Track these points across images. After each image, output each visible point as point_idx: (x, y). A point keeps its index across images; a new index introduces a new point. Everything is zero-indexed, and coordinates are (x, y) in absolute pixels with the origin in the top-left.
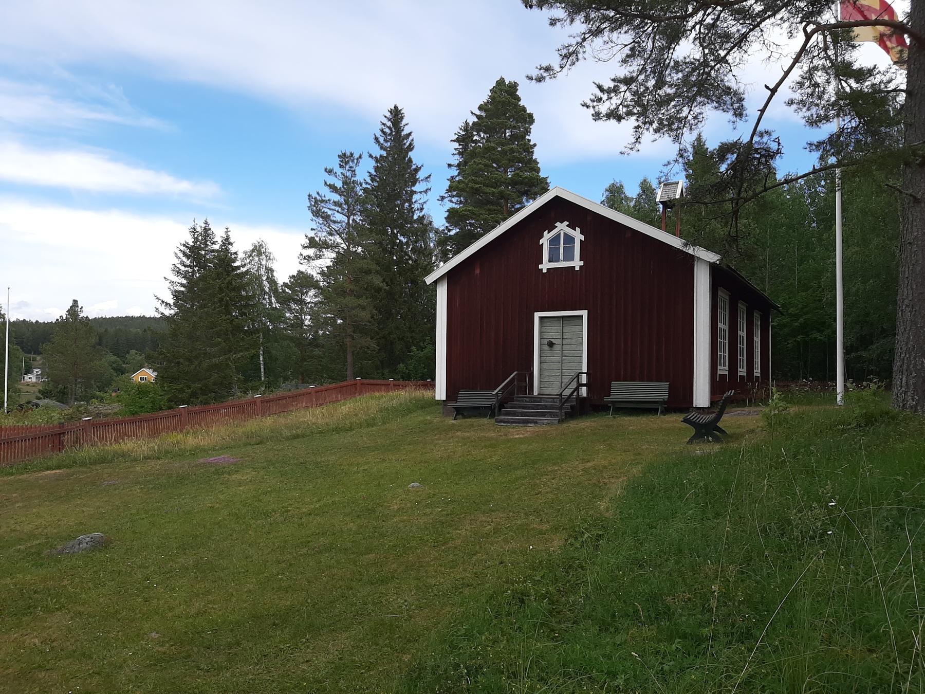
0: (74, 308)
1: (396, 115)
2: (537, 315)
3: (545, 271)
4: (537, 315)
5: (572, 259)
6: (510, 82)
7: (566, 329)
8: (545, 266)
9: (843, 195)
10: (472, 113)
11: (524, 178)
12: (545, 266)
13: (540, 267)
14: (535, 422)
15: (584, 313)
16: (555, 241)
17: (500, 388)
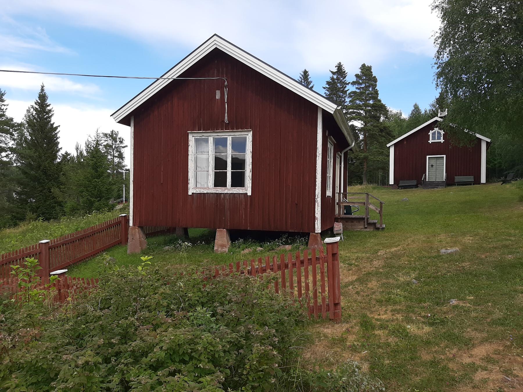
0: (124, 157)
1: (305, 72)
2: (428, 157)
3: (444, 141)
4: (428, 157)
5: (440, 139)
6: (377, 89)
8: (430, 141)
10: (330, 71)
11: (378, 105)
12: (430, 141)
13: (442, 142)
14: (437, 188)
15: (445, 156)
16: (434, 134)
17: (131, 218)
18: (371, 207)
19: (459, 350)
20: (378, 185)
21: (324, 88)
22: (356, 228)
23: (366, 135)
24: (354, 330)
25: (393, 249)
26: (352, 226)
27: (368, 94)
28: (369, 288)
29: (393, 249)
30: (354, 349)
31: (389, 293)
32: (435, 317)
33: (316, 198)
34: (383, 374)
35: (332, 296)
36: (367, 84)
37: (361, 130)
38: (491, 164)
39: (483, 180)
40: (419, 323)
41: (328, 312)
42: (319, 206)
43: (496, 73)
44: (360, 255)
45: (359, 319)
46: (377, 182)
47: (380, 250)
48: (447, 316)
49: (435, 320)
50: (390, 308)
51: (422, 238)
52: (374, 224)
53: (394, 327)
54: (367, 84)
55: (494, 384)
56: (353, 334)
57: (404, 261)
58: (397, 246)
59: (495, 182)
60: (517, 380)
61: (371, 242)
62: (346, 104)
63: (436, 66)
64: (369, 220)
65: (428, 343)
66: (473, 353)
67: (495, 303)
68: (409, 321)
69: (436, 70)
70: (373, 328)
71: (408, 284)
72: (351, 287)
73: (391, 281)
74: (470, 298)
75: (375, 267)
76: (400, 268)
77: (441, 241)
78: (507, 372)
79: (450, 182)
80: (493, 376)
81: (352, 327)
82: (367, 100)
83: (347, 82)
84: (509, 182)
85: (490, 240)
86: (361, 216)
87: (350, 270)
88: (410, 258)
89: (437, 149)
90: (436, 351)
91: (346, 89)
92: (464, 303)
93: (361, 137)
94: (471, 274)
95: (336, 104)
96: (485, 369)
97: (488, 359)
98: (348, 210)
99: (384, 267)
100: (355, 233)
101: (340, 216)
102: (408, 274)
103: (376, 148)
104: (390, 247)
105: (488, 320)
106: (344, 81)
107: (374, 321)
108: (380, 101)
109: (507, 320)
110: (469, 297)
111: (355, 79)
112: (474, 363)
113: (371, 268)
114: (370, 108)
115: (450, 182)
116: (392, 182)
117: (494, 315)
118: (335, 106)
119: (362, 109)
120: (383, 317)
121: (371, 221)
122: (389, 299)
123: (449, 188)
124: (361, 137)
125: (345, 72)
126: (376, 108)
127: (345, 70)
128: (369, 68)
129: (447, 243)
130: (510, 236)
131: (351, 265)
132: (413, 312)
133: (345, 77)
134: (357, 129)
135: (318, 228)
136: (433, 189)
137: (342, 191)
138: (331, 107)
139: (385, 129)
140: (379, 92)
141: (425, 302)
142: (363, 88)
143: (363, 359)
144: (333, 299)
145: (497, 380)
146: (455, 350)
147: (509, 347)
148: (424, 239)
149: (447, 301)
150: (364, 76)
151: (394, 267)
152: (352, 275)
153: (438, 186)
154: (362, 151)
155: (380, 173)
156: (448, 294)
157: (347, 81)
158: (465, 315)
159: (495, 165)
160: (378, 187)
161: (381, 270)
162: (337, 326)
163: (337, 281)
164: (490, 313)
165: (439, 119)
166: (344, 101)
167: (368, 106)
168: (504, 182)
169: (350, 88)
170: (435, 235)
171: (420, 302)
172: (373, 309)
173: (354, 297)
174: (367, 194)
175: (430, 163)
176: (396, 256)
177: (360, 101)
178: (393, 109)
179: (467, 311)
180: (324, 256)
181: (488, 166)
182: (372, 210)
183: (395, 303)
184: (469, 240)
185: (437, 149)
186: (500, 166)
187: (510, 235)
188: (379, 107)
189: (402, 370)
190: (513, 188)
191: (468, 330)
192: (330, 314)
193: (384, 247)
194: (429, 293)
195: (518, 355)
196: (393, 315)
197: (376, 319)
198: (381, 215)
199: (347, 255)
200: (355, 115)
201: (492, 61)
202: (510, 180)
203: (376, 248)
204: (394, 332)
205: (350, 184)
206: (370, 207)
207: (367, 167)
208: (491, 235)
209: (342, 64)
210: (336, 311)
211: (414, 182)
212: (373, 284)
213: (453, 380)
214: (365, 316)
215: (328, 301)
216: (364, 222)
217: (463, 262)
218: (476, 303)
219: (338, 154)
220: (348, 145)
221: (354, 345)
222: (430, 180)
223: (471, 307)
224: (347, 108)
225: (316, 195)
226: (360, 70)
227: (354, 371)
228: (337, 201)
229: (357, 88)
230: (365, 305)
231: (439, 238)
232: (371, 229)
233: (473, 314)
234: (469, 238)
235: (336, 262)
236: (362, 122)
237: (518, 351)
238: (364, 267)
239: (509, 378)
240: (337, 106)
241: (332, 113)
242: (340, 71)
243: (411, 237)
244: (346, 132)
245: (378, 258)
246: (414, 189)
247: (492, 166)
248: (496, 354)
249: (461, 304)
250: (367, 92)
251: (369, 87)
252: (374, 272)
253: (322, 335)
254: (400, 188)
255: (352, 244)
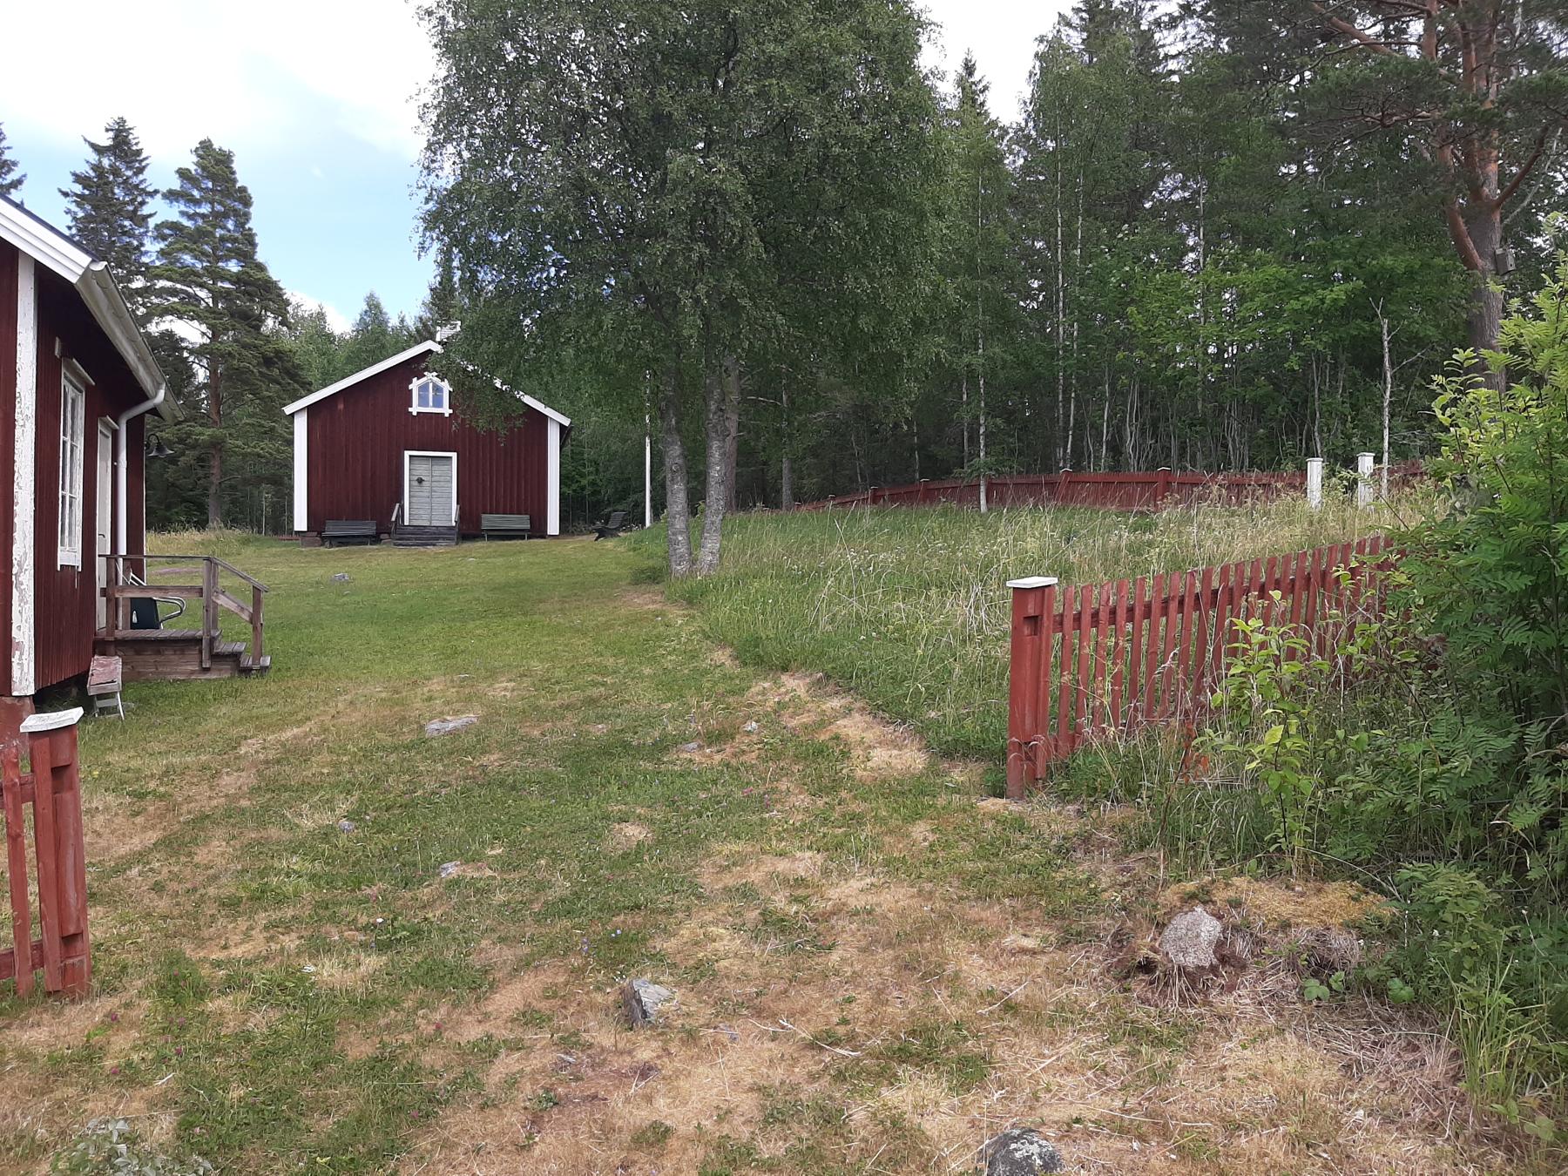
2: (407, 454)
4: (407, 454)
6: (250, 229)
7: (435, 468)
8: (415, 409)
9: (533, 394)
12: (415, 409)
15: (454, 455)
16: (423, 388)
18: (222, 601)
19: (455, 1006)
20: (260, 532)
21: (66, 194)
22: (170, 673)
23: (215, 371)
24: (133, 1014)
25: (288, 734)
26: (156, 665)
27: (223, 239)
28: (197, 866)
29: (288, 734)
30: (128, 1077)
31: (263, 873)
32: (395, 924)
33: (14, 571)
34: (220, 1137)
35: (55, 912)
36: (218, 208)
37: (199, 352)
38: (574, 486)
39: (553, 526)
40: (348, 950)
41: (40, 971)
42: (26, 603)
43: (576, 241)
44: (175, 760)
45: (155, 972)
46: (255, 523)
47: (246, 738)
48: (430, 915)
49: (395, 933)
50: (262, 918)
51: (379, 691)
52: (235, 656)
53: (268, 977)
54: (218, 208)
55: (535, 1081)
56: (131, 1029)
57: (319, 765)
58: (300, 723)
59: (581, 533)
60: (589, 1056)
61: (220, 716)
62: (145, 259)
63: (424, 193)
64: (216, 644)
65: (369, 1005)
66: (490, 1009)
67: (555, 857)
68: (318, 948)
69: (418, 206)
70: (201, 993)
71: (327, 834)
72: (135, 871)
73: (274, 832)
74: (493, 852)
75: (227, 796)
76: (307, 788)
77: (430, 699)
78: (569, 1042)
79: (468, 530)
80: (535, 1062)
81: (127, 1006)
82: (219, 259)
83: (150, 189)
84: (613, 535)
85: (557, 688)
86: (191, 633)
87: (138, 814)
88: (338, 755)
89: (431, 434)
90: (388, 1026)
91: (145, 211)
92: (479, 869)
93: (201, 375)
94: (502, 784)
95: (87, 252)
96: (516, 1046)
97: (529, 1017)
98: (146, 612)
99: (255, 790)
100: (167, 690)
101: (112, 635)
102: (329, 804)
103: (250, 416)
104: (282, 724)
105: (536, 907)
106: (135, 180)
107: (205, 971)
108: (261, 268)
109: (579, 899)
110: (492, 849)
111: (176, 184)
112: (490, 1037)
113: (210, 798)
114: (227, 285)
115: (468, 530)
116: (300, 522)
117: (550, 892)
118: (85, 260)
119: (202, 286)
120: (237, 952)
121: (223, 647)
122: (262, 892)
123: (466, 545)
124: (201, 375)
125: (139, 152)
126: (249, 288)
127: (139, 147)
128: (224, 159)
129: (447, 703)
130: (603, 675)
131: (141, 796)
132: (333, 919)
133: (141, 170)
134: (186, 348)
135: (24, 678)
136: (421, 549)
137: (123, 550)
138: (71, 263)
139: (280, 359)
140: (257, 240)
141: (371, 883)
142: (203, 216)
143: (163, 1102)
144: (56, 921)
145: (543, 1070)
146: (443, 1010)
147: (578, 972)
148: (384, 695)
149: (433, 870)
150: (207, 178)
151: (286, 788)
152: (144, 829)
153: (437, 539)
154: (205, 421)
155: (266, 496)
156: (436, 852)
157: (148, 183)
158: (477, 902)
159: (583, 488)
160: (257, 540)
161: (244, 803)
162: (71, 1011)
163: (70, 862)
164: (541, 887)
165: (437, 348)
166: (137, 248)
167: (223, 279)
168: (602, 534)
169: (161, 211)
170: (415, 683)
171: (358, 884)
172: (206, 933)
173: (147, 901)
174: (208, 559)
175: (414, 472)
176: (297, 753)
177: (195, 257)
178: (302, 296)
179: (484, 891)
180: (20, 778)
181: (565, 489)
182: (228, 612)
183: (281, 900)
184: (505, 689)
185: (431, 434)
186: (595, 493)
187: (603, 671)
188: (258, 287)
189: (284, 1107)
190: (622, 549)
191: (484, 943)
192: (45, 976)
193: (259, 729)
194: (385, 854)
195: (598, 989)
196: (270, 939)
197: (212, 964)
198: (255, 628)
199: (134, 764)
200: (176, 300)
201: (567, 207)
202: (617, 529)
203: (234, 732)
204: (272, 994)
205: (161, 523)
206: (219, 602)
207: (224, 474)
208: (560, 673)
209: (129, 125)
210: (71, 961)
211: (369, 528)
212: (215, 850)
213: (430, 1101)
214: (176, 959)
215: (39, 930)
216: (201, 652)
217: (484, 752)
218: (509, 864)
219: (106, 425)
220: (143, 396)
221: (129, 1064)
222: (415, 523)
223: (494, 878)
224: (149, 272)
225: (15, 562)
226: (195, 159)
227: (114, 1154)
228: (101, 580)
229: (183, 213)
230: (179, 922)
231: (426, 689)
232: (221, 674)
233: (500, 897)
234: (505, 684)
235: (67, 796)
236: (204, 328)
237: (600, 977)
238: (189, 799)
239: (571, 1055)
240: (93, 261)
241: (73, 279)
242: (122, 146)
243: (346, 692)
244: (131, 352)
245: (236, 764)
246: (369, 547)
247: (574, 491)
248: (548, 998)
249: (471, 873)
250: (219, 232)
251: (225, 215)
252: (219, 812)
253: (10, 1055)
254: (327, 543)
255: (151, 727)
